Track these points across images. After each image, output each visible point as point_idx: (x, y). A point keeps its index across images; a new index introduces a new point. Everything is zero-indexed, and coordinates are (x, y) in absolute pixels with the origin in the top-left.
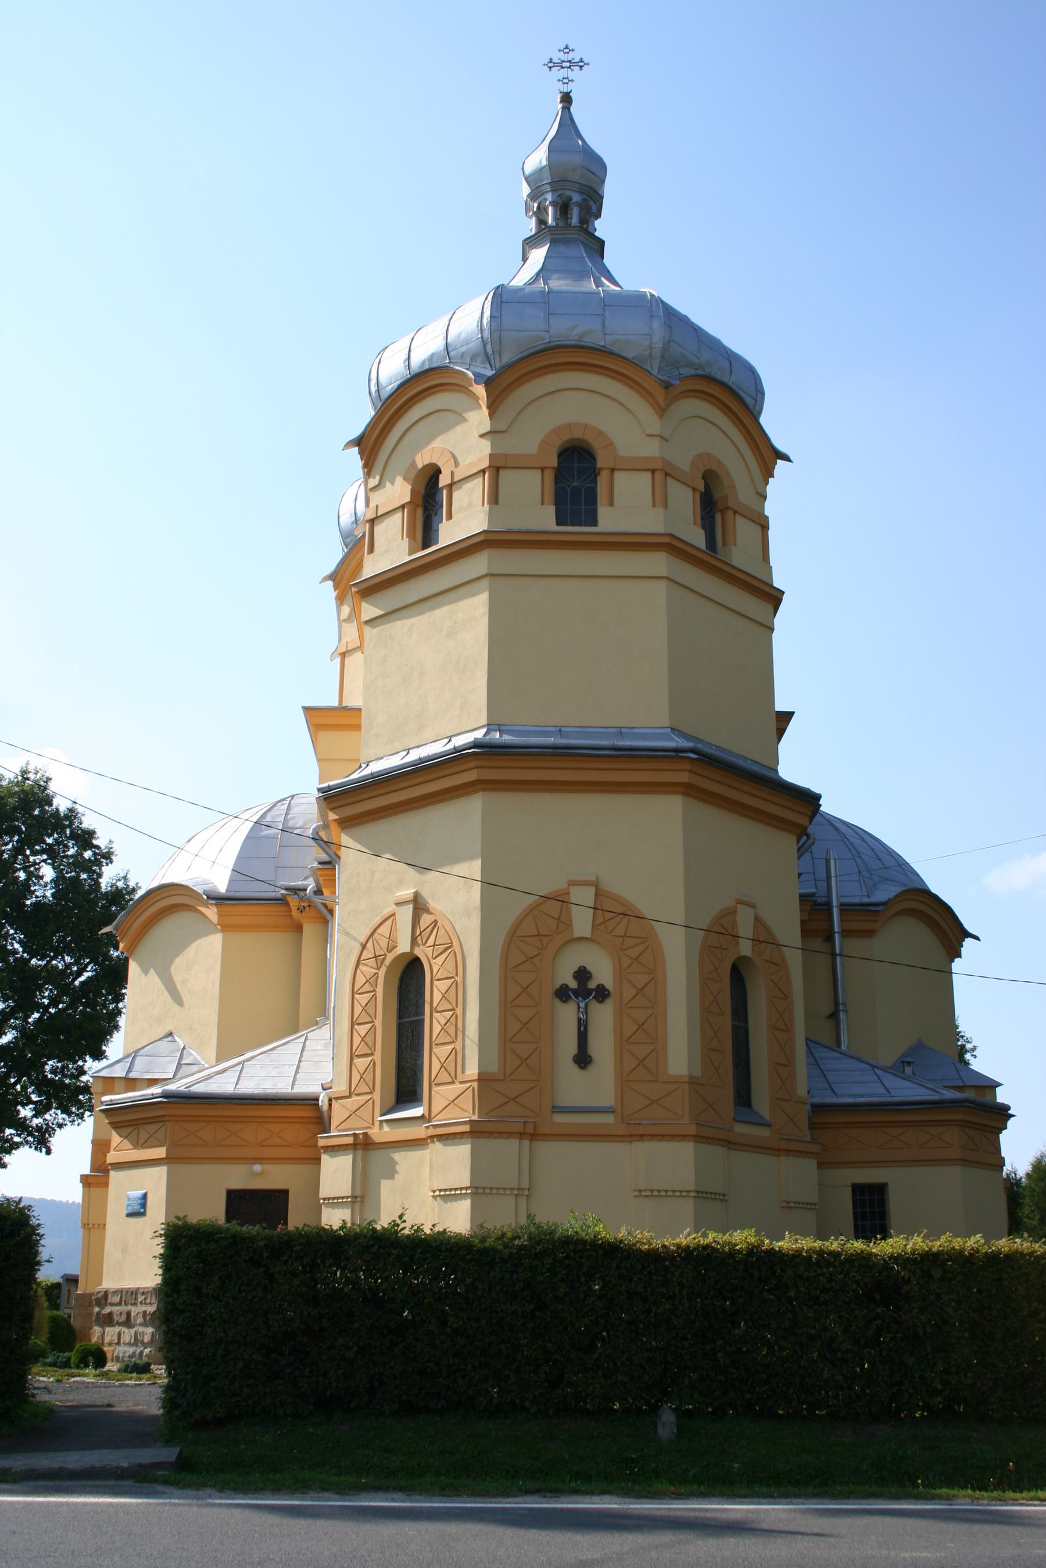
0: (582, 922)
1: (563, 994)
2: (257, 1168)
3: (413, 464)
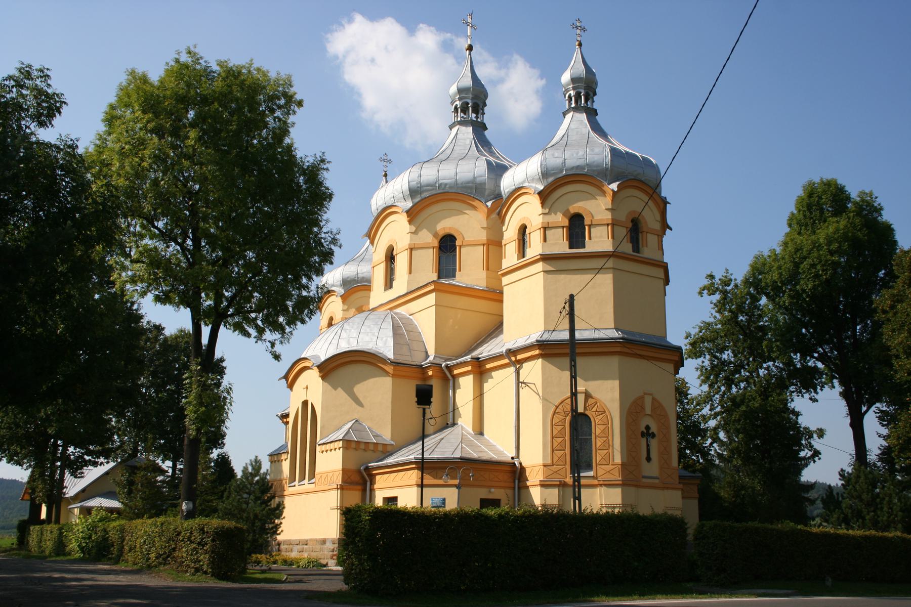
0: (648, 410)
1: (643, 435)
2: (493, 490)
3: (568, 210)
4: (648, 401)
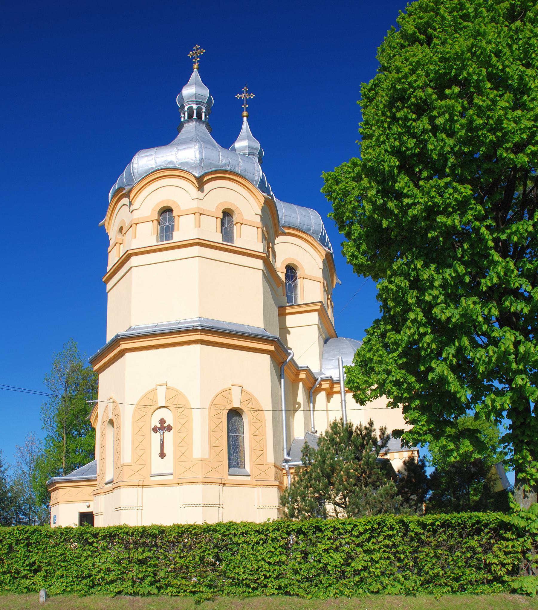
1: (155, 430)
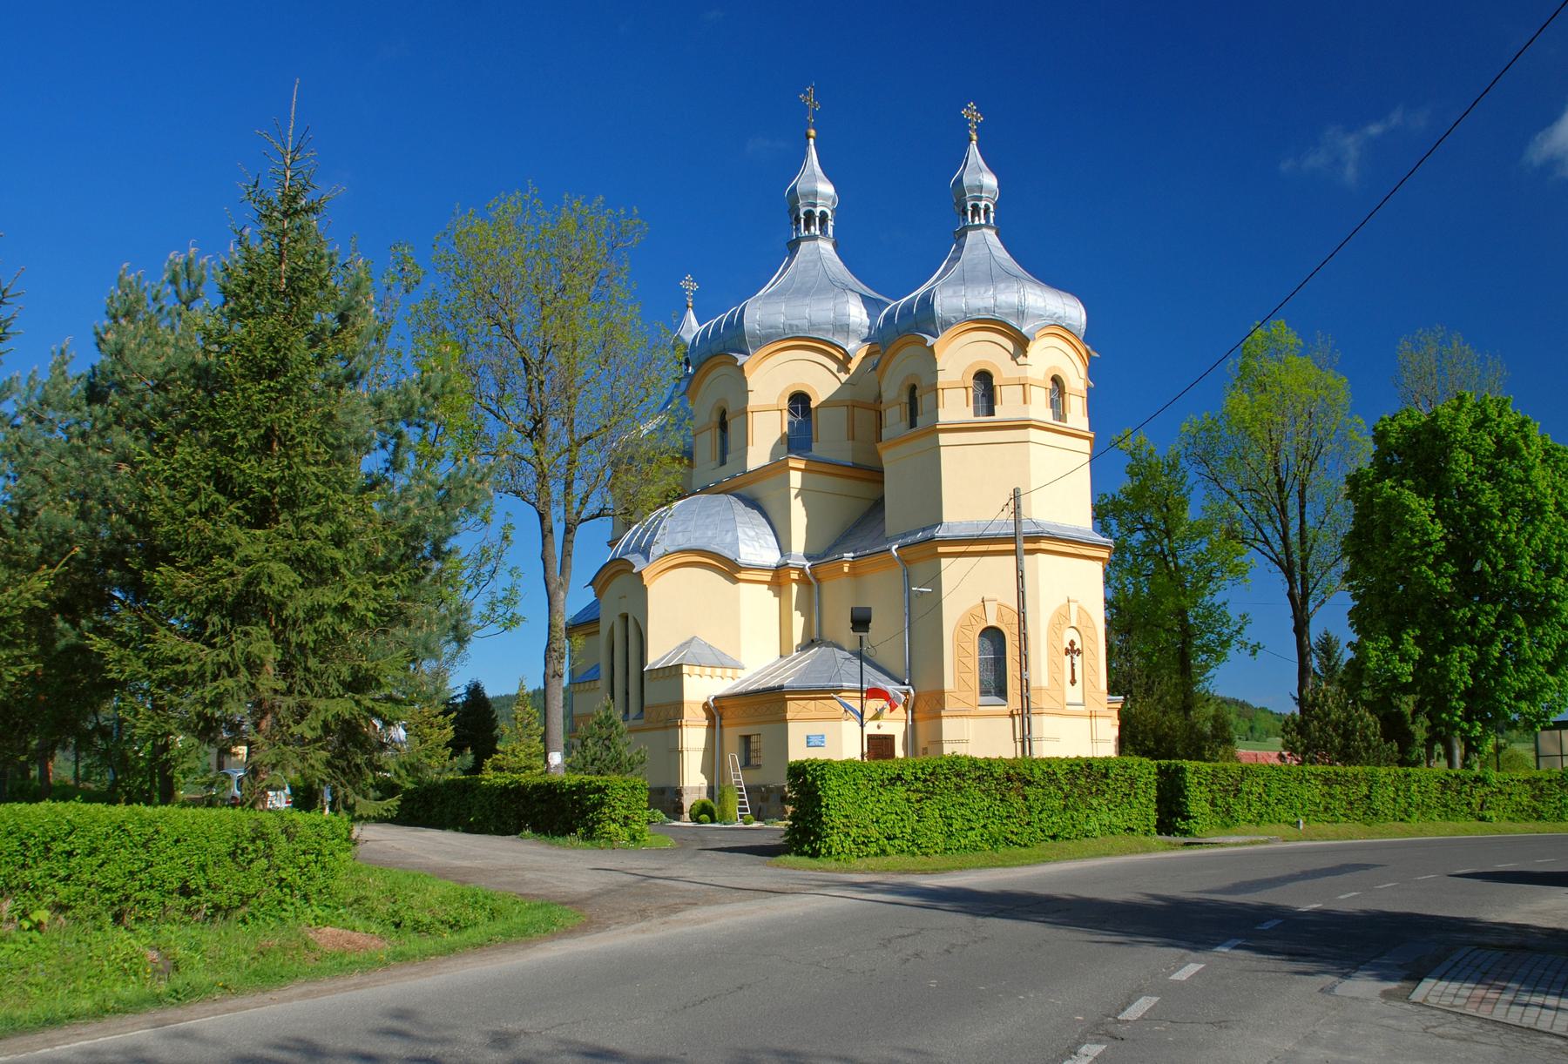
4: (1073, 607)
